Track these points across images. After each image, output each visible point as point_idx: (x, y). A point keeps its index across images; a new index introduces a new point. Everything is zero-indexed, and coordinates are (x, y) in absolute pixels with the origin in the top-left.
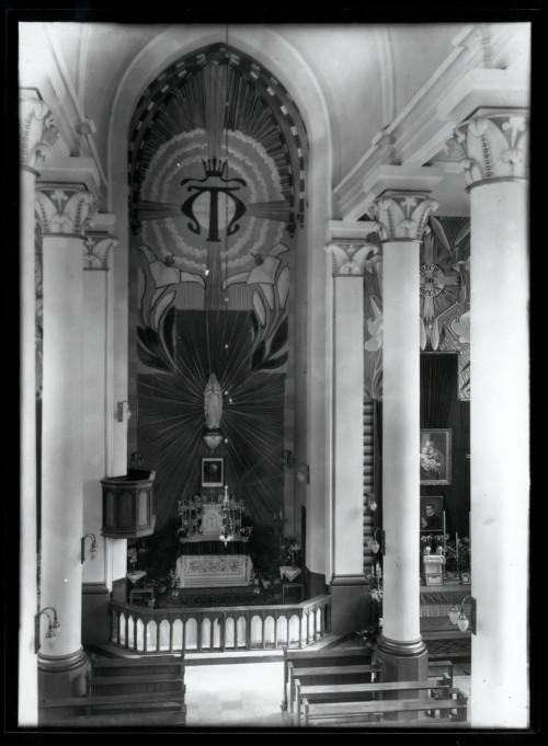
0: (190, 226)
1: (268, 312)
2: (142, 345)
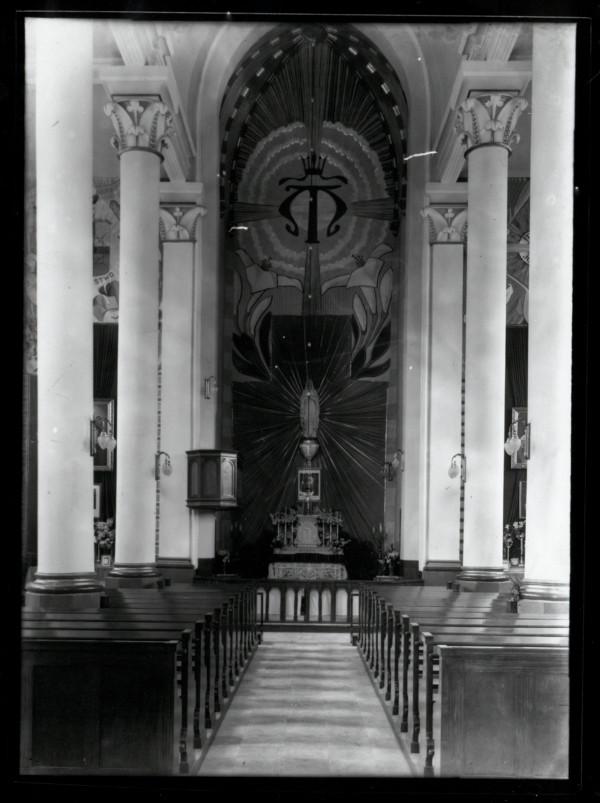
0: (288, 228)
1: (370, 317)
2: (238, 352)
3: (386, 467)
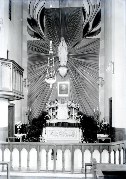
1: (91, 7)
3: (100, 79)
